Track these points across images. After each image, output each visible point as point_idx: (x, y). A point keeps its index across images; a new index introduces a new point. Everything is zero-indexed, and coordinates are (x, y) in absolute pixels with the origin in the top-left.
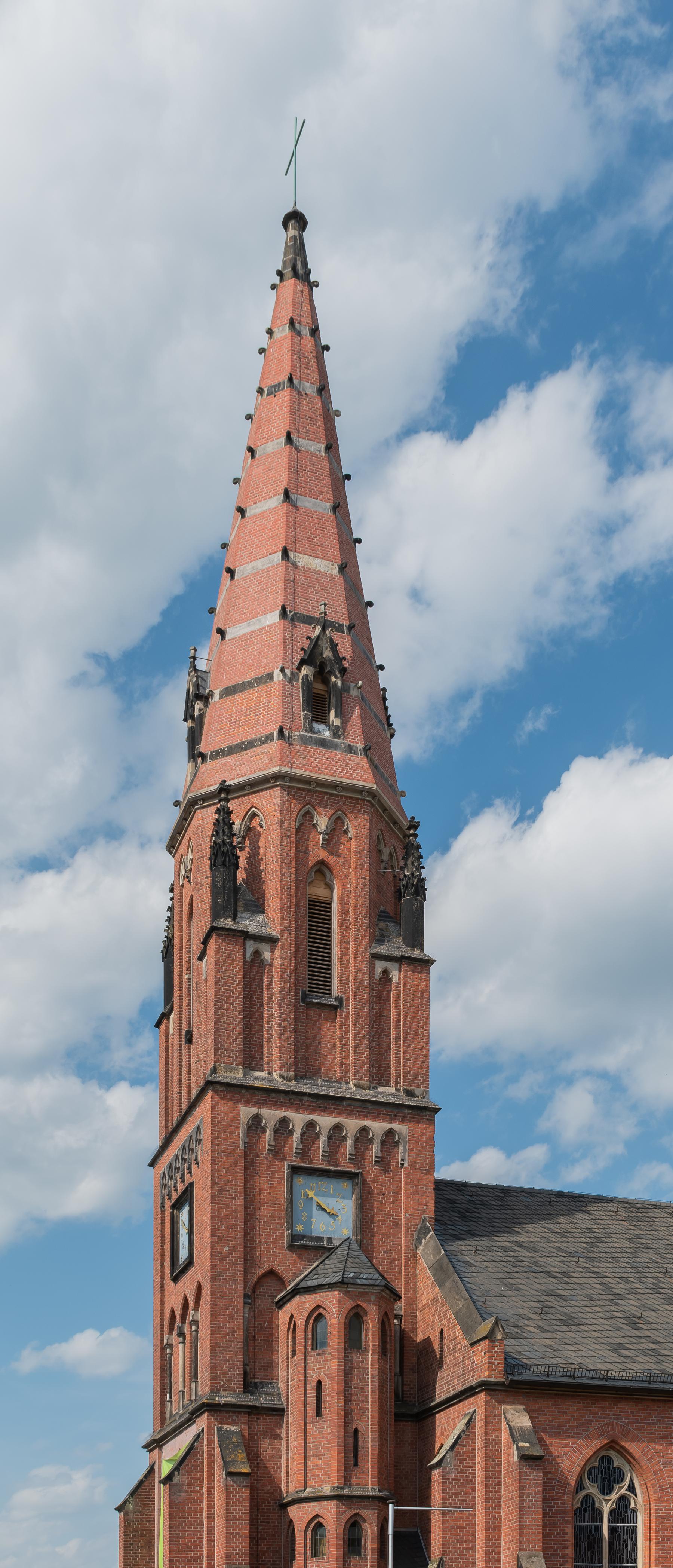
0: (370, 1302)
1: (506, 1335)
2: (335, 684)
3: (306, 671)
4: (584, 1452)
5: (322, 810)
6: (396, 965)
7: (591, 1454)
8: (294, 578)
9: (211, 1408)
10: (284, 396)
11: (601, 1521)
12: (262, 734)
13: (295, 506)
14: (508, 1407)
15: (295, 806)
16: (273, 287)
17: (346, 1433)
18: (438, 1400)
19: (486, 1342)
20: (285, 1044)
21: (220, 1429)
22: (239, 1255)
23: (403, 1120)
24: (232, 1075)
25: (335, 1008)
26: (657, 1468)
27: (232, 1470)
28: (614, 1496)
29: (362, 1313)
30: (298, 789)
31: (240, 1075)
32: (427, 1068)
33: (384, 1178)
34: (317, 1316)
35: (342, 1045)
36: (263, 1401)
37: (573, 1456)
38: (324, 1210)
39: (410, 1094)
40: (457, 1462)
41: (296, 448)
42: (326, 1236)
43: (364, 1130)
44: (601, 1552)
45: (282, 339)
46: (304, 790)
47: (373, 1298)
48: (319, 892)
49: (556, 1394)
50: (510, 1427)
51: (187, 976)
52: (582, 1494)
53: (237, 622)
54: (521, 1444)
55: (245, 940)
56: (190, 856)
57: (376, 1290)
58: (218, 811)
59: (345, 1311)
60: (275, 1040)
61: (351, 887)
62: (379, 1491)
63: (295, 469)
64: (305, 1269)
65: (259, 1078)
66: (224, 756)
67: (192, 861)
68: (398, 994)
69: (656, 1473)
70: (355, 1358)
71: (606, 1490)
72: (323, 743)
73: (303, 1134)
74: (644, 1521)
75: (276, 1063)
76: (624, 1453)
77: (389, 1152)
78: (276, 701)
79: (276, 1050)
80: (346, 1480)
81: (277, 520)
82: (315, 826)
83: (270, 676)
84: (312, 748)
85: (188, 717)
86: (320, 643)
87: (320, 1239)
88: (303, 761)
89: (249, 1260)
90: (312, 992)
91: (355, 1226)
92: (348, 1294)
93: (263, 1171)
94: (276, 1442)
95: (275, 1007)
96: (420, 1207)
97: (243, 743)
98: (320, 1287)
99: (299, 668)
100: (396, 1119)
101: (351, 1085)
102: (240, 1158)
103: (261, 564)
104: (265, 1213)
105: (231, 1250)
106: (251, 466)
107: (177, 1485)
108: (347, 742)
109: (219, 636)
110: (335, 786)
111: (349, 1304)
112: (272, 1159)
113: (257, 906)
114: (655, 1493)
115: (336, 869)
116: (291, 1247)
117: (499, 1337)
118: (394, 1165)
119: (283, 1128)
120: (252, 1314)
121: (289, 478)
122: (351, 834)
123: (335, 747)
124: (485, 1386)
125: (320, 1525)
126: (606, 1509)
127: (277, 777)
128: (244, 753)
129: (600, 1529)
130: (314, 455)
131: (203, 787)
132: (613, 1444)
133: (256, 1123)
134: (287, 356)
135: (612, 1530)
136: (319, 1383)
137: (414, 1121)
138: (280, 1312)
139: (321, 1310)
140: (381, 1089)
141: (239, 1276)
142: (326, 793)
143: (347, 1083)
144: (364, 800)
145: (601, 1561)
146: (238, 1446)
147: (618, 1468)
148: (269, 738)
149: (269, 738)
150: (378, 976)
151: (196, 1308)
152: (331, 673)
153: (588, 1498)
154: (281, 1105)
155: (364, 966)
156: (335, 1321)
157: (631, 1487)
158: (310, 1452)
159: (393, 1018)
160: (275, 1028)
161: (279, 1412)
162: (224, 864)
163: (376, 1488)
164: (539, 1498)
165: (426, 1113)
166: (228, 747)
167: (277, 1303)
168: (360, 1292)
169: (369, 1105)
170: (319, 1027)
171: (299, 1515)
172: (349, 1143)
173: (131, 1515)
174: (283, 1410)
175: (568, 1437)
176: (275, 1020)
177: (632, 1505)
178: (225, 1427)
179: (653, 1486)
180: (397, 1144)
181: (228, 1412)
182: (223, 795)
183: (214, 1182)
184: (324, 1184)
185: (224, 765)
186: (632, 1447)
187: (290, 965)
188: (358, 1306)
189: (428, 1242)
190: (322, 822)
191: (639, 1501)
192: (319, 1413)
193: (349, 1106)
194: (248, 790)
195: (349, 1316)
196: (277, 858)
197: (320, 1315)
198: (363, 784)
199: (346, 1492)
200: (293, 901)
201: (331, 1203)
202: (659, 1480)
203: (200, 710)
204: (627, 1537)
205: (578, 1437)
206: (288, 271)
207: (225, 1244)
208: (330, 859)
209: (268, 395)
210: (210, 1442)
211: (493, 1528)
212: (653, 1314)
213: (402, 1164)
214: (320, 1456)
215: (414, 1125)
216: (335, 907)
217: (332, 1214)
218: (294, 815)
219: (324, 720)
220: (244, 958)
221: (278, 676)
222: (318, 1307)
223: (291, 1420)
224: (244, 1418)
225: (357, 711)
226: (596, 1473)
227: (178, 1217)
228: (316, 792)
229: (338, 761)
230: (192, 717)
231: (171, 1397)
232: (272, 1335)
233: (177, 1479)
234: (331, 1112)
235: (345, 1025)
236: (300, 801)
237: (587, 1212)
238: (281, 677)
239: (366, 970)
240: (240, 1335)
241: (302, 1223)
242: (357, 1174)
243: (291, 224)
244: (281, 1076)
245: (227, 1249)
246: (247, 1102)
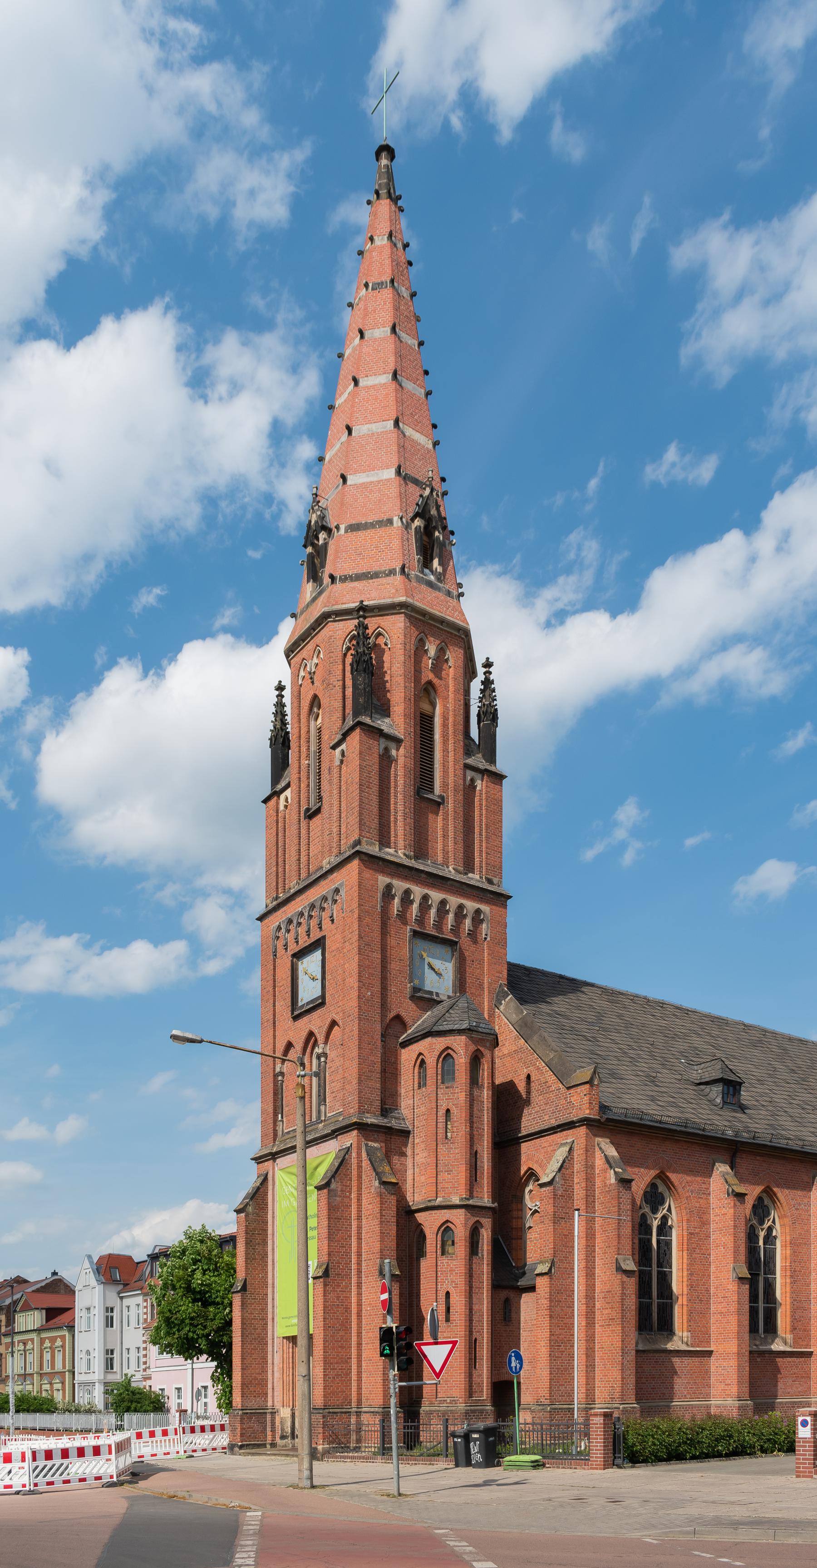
0: (485, 1047)
1: (601, 1081)
2: (438, 538)
3: (418, 522)
5: (432, 639)
6: (480, 776)
8: (404, 446)
9: (361, 1127)
10: (387, 294)
12: (386, 568)
13: (401, 385)
14: (600, 1139)
16: (369, 202)
18: (524, 1132)
19: (587, 1086)
20: (407, 828)
21: (366, 1145)
22: (377, 1000)
26: (687, 1194)
27: (385, 1180)
28: (659, 1215)
29: (480, 1056)
30: (416, 618)
31: (377, 849)
32: (501, 862)
33: (473, 948)
34: (446, 1056)
35: (443, 828)
36: (394, 1124)
39: (490, 881)
40: (562, 1182)
41: (399, 338)
42: (434, 990)
44: (651, 1259)
45: (383, 246)
46: (420, 620)
47: (488, 1044)
48: (426, 707)
50: (606, 1156)
51: (307, 762)
53: (356, 472)
54: (617, 1170)
56: (315, 660)
58: (357, 627)
59: (469, 1053)
60: (400, 823)
61: (451, 706)
63: (399, 357)
64: (421, 1016)
65: (389, 853)
66: (352, 580)
67: (317, 665)
68: (481, 800)
71: (655, 1211)
72: (430, 584)
74: (678, 1235)
75: (401, 843)
78: (396, 543)
79: (400, 832)
81: (387, 394)
83: (390, 522)
84: (424, 587)
85: (309, 543)
87: (431, 993)
89: (384, 1006)
91: (454, 986)
92: (471, 1038)
94: (403, 1159)
95: (400, 796)
96: (497, 975)
97: (369, 573)
98: (451, 1032)
99: (413, 520)
101: (451, 868)
102: (378, 918)
103: (376, 427)
104: (394, 966)
106: (360, 345)
107: (333, 1190)
109: (341, 480)
110: (442, 621)
111: (473, 1048)
113: (382, 710)
115: (440, 690)
116: (412, 998)
117: (596, 1083)
121: (396, 362)
123: (438, 589)
124: (586, 1122)
125: (448, 1229)
127: (402, 605)
128: (370, 581)
129: (650, 1240)
130: (411, 347)
131: (337, 604)
134: (388, 262)
135: (658, 1241)
138: (403, 1051)
139: (450, 1051)
140: (470, 875)
141: (378, 1017)
142: (435, 626)
143: (448, 867)
145: (651, 1266)
146: (383, 1160)
147: (661, 1193)
148: (392, 572)
149: (392, 572)
150: (468, 783)
151: (326, 1043)
152: (435, 528)
155: (460, 773)
156: (463, 1060)
157: (669, 1210)
158: (440, 1168)
159: (477, 818)
160: (400, 813)
161: (405, 1134)
162: (365, 671)
165: (500, 899)
166: (356, 574)
167: (401, 1043)
168: (480, 1039)
169: (464, 887)
171: (430, 1222)
173: (251, 1216)
174: (408, 1132)
176: (400, 808)
177: (670, 1223)
178: (370, 1143)
179: (686, 1208)
180: (482, 921)
181: (371, 1131)
182: (361, 613)
183: (360, 937)
185: (354, 588)
186: (673, 1177)
187: (411, 764)
188: (478, 1049)
189: (508, 1003)
190: (432, 649)
193: (452, 885)
194: (376, 612)
196: (401, 672)
197: (448, 1054)
199: (471, 1202)
201: (437, 964)
203: (325, 539)
206: (383, 192)
207: (368, 989)
208: (436, 681)
209: (373, 289)
210: (359, 1155)
211: (590, 1235)
213: (486, 939)
214: (449, 1172)
215: (494, 907)
216: (438, 721)
218: (413, 639)
221: (397, 522)
222: (448, 1048)
223: (417, 1141)
224: (382, 1137)
227: (297, 965)
228: (428, 623)
229: (442, 601)
230: (313, 545)
231: (282, 1117)
232: (397, 1069)
233: (333, 1186)
234: (405, 878)
235: (445, 819)
236: (417, 629)
237: (583, 992)
238: (400, 524)
240: (378, 1067)
242: (456, 943)
243: (384, 154)
244: (405, 854)
246: (383, 872)
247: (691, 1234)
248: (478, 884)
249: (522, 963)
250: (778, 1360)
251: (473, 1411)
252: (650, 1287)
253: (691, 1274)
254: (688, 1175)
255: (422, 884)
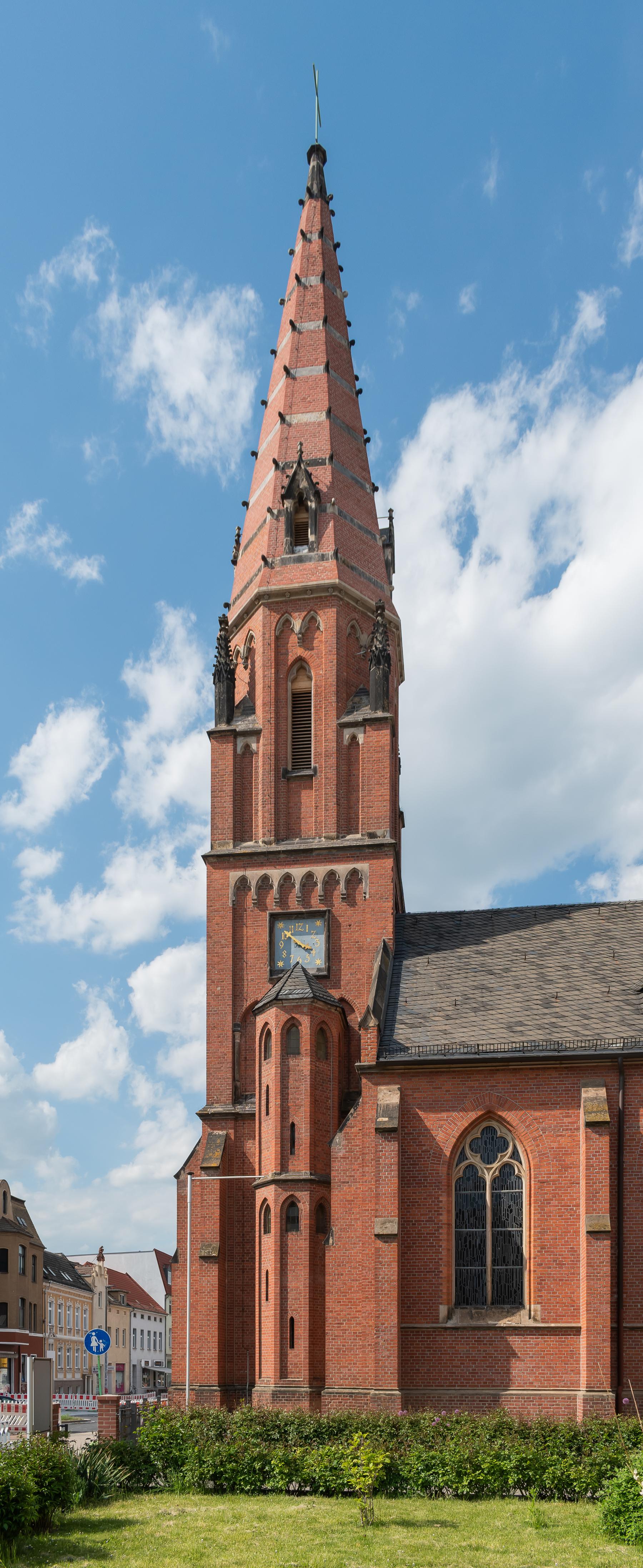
0: (302, 1013)
4: (459, 1124)
6: (362, 729)
7: (466, 1125)
11: (484, 1188)
15: (275, 617)
17: (282, 1127)
22: (228, 992)
23: (365, 859)
24: (225, 848)
25: (311, 776)
26: (536, 1134)
30: (277, 603)
33: (350, 911)
35: (317, 808)
37: (446, 1128)
38: (300, 946)
40: (344, 1142)
43: (332, 874)
44: (484, 1218)
46: (282, 602)
47: (305, 1010)
49: (431, 1072)
52: (466, 1163)
55: (235, 738)
57: (306, 1002)
62: (311, 1174)
69: (535, 1139)
70: (292, 1062)
71: (489, 1160)
73: (281, 886)
76: (502, 1121)
77: (355, 889)
80: (283, 1166)
82: (292, 630)
86: (297, 477)
88: (279, 578)
90: (293, 767)
92: (284, 1009)
93: (249, 922)
96: (380, 931)
100: (358, 859)
105: (223, 990)
108: (320, 553)
110: (305, 590)
111: (285, 1017)
112: (257, 911)
114: (533, 1159)
115: (310, 661)
118: (359, 898)
119: (265, 881)
120: (244, 1039)
122: (322, 628)
126: (488, 1178)
132: (489, 1115)
133: (243, 883)
135: (496, 1197)
136: (268, 1086)
137: (374, 859)
141: (229, 1009)
142: (300, 600)
144: (331, 596)
153: (471, 1167)
154: (262, 865)
155: (332, 736)
157: (515, 1155)
160: (260, 803)
163: (308, 1172)
164: (395, 1168)
169: (334, 851)
170: (300, 796)
172: (320, 886)
175: (443, 1111)
181: (218, 1120)
184: (299, 925)
186: (509, 1116)
188: (293, 1018)
190: (297, 624)
191: (523, 1169)
192: (267, 1114)
193: (318, 855)
195: (286, 1028)
198: (327, 581)
200: (273, 695)
202: (538, 1146)
204: (512, 1203)
205: (454, 1111)
212: (577, 993)
215: (375, 861)
217: (307, 949)
219: (305, 542)
220: (235, 750)
224: (231, 1124)
225: (331, 524)
226: (480, 1144)
228: (291, 601)
234: (302, 863)
239: (334, 739)
241: (283, 960)
242: (325, 912)
244: (264, 842)
245: (219, 988)
246: (235, 867)
247: (542, 1182)
248: (359, 843)
249: (530, 905)
250: (510, 1339)
251: (284, 1392)
252: (484, 1253)
253: (543, 1232)
254: (535, 1110)
255: (282, 865)
